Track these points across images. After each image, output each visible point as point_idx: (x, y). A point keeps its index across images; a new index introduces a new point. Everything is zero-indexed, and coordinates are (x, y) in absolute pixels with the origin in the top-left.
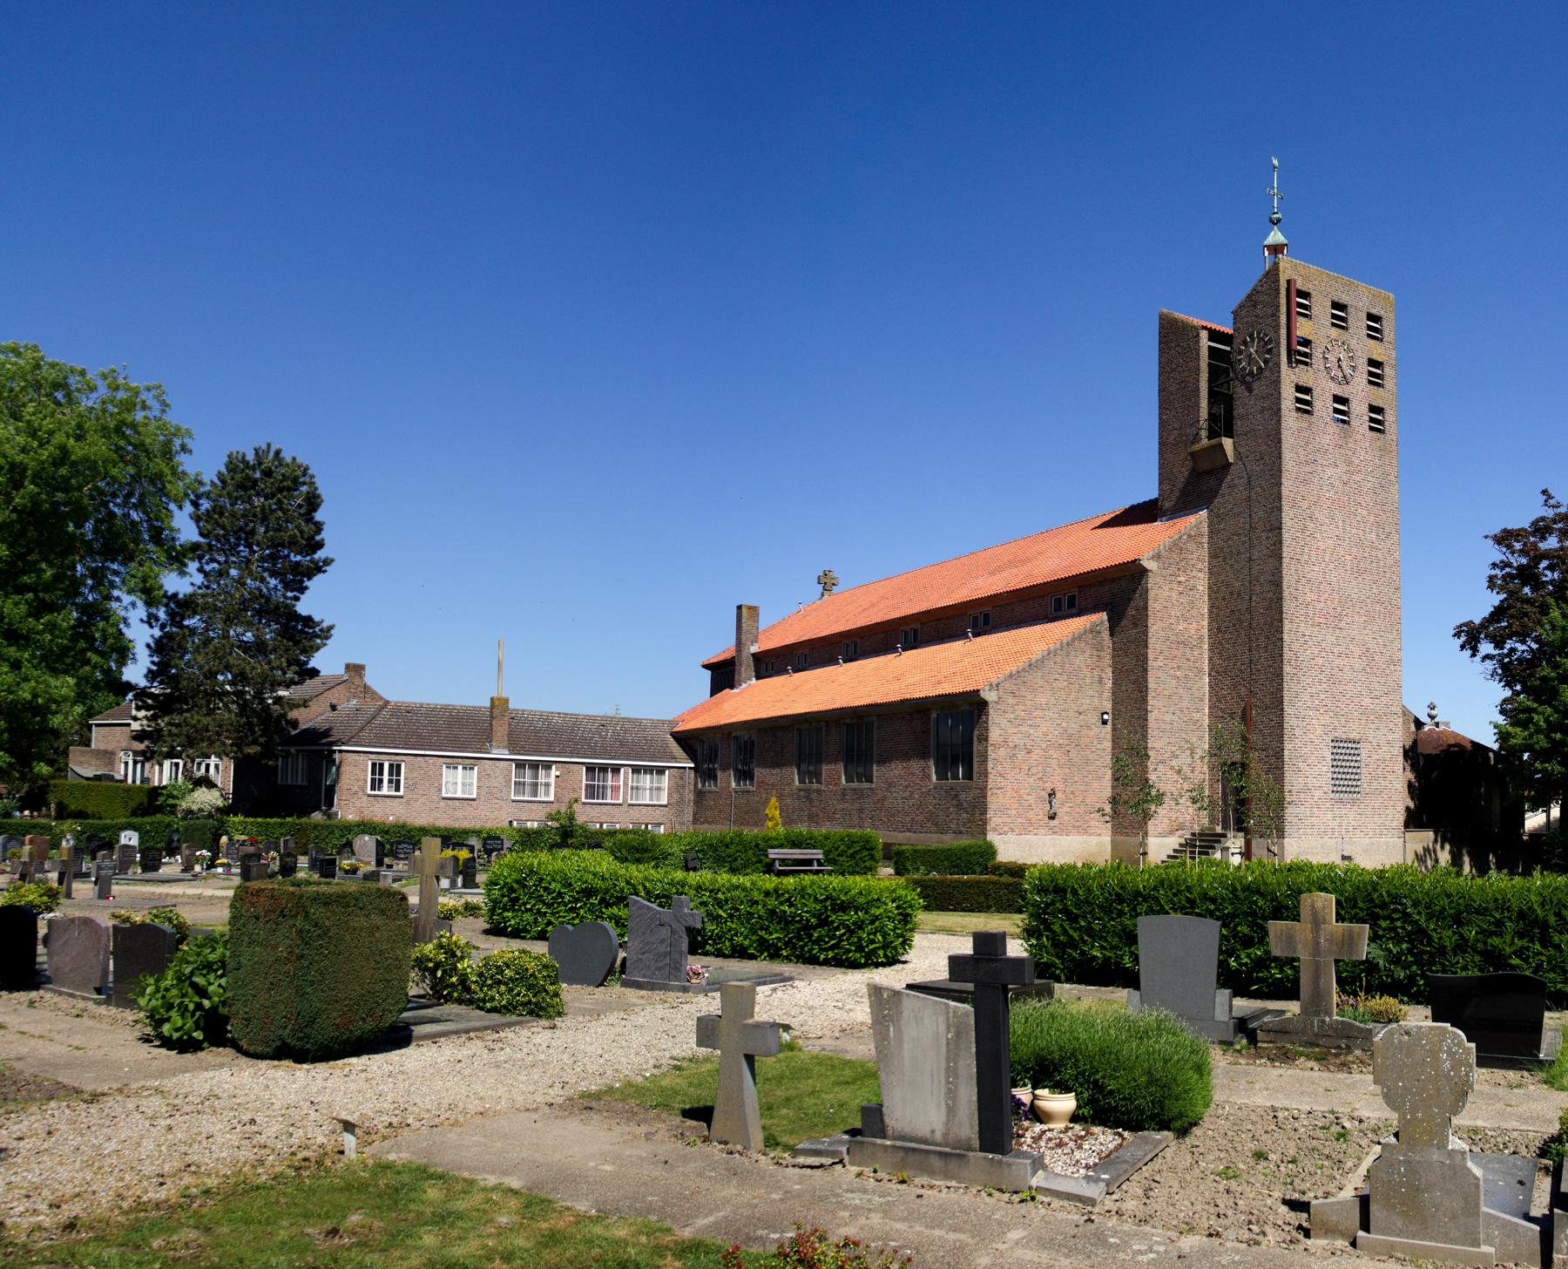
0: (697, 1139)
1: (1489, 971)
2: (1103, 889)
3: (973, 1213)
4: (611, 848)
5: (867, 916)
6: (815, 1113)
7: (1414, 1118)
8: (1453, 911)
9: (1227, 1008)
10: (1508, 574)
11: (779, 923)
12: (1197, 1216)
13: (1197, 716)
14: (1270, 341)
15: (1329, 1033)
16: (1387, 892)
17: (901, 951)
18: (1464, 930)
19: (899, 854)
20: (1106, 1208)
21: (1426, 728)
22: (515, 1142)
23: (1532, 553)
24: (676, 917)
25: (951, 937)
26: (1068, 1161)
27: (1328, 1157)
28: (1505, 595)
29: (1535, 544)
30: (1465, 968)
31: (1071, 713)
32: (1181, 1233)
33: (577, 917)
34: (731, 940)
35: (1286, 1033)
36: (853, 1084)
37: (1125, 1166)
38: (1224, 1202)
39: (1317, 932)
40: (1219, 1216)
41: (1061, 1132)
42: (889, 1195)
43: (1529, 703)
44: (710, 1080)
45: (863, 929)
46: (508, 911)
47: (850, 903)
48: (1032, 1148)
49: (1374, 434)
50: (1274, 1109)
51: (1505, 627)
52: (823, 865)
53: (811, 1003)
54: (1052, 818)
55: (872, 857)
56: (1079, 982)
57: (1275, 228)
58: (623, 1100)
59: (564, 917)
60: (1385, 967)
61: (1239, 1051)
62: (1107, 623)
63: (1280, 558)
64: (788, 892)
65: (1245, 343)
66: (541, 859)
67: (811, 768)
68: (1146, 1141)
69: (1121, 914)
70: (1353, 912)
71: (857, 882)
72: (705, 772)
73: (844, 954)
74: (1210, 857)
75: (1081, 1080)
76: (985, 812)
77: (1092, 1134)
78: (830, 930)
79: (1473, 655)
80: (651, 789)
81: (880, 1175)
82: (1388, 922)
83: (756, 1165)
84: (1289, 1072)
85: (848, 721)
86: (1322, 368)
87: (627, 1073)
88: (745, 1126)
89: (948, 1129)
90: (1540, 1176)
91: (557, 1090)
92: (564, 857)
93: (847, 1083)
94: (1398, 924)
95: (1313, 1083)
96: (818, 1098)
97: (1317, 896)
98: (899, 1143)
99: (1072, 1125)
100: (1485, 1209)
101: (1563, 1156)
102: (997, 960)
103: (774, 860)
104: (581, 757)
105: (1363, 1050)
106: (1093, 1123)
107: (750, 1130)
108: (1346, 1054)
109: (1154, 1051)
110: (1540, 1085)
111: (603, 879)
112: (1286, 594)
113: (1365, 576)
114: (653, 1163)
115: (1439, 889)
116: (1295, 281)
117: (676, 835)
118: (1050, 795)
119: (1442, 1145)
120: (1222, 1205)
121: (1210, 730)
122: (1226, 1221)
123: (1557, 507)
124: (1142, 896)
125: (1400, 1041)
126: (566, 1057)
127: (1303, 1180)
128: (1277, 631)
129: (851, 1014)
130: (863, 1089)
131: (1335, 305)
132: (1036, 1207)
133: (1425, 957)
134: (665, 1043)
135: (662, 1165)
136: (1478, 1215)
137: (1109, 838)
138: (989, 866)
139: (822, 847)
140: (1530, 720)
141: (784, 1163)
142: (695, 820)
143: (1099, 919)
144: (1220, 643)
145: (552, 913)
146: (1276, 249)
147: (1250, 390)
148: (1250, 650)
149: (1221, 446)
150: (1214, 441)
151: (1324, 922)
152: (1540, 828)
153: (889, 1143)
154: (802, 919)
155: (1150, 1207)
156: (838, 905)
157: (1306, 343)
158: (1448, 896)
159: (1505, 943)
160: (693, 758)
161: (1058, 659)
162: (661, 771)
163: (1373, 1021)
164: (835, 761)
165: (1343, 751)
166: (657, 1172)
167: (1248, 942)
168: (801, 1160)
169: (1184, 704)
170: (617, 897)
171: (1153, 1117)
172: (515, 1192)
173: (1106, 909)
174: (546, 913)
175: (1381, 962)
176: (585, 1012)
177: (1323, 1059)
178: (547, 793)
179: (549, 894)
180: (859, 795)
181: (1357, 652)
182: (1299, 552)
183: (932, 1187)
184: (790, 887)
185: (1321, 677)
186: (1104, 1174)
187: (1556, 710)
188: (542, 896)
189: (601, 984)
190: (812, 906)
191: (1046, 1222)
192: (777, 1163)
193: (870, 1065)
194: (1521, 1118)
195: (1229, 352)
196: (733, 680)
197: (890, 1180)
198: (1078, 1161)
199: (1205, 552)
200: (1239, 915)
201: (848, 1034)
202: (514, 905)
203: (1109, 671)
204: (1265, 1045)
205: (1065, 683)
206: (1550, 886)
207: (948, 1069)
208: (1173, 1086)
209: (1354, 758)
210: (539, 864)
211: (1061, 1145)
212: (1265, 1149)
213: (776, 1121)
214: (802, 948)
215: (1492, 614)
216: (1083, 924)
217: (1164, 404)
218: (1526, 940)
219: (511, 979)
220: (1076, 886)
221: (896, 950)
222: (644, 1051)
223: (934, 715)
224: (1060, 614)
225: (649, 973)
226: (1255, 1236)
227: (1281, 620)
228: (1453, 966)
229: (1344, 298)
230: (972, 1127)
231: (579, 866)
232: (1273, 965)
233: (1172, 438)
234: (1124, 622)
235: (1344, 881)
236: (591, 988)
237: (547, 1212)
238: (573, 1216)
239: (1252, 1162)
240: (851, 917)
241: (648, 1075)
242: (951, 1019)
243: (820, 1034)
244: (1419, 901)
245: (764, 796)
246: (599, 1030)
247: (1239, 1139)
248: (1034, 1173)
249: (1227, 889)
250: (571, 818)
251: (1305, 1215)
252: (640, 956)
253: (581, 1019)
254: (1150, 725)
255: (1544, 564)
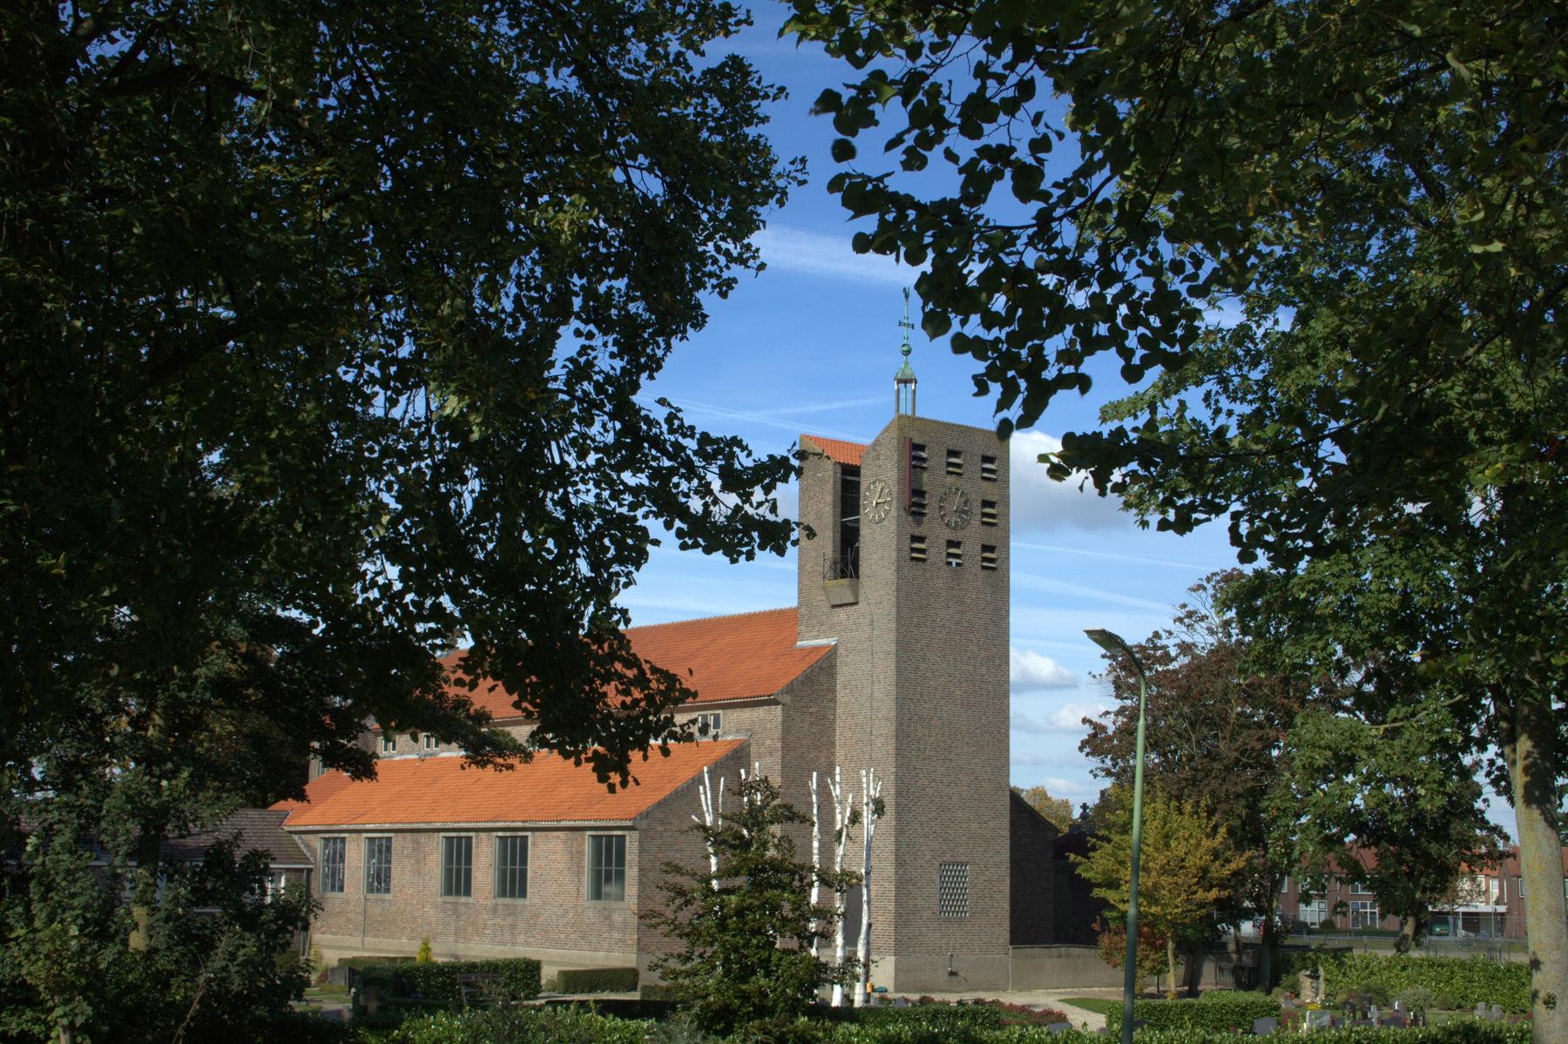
49: (986, 572)
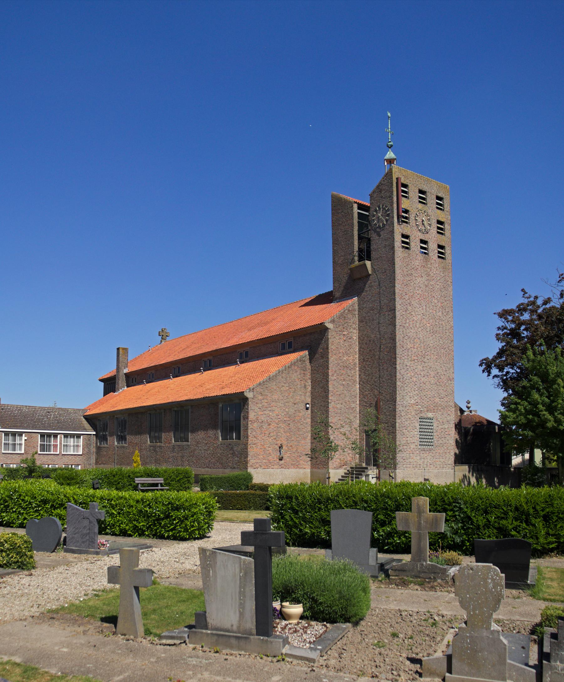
0: (110, 633)
1: (500, 538)
2: (311, 496)
3: (253, 668)
4: (55, 478)
5: (190, 513)
6: (169, 617)
7: (474, 613)
8: (483, 507)
9: (375, 558)
10: (505, 333)
11: (144, 517)
12: (366, 667)
13: (353, 405)
14: (388, 210)
15: (425, 571)
16: (452, 497)
17: (207, 531)
18: (488, 516)
19: (202, 480)
20: (320, 664)
21: (465, 414)
22: (15, 637)
23: (517, 322)
24: (91, 514)
25: (231, 523)
26: (300, 640)
27: (428, 635)
28: (505, 344)
29: (518, 317)
30: (489, 536)
31: (291, 404)
32: (358, 676)
33: (39, 515)
34: (119, 526)
35: (404, 571)
36: (187, 602)
37: (329, 642)
38: (378, 659)
39: (420, 518)
40: (376, 667)
41: (296, 625)
42: (210, 659)
43: (516, 400)
44: (114, 601)
45: (188, 520)
46: (4, 512)
47: (181, 506)
48: (281, 633)
49: (440, 260)
50: (400, 611)
51: (504, 361)
52: (163, 486)
53: (162, 560)
54: (281, 459)
55: (189, 482)
56: (299, 546)
57: (390, 150)
58: (70, 613)
59: (33, 515)
60: (450, 536)
61: (381, 581)
62: (308, 356)
63: (395, 326)
64: (148, 500)
65: (376, 211)
66: (20, 483)
67: (156, 434)
68: (338, 628)
69: (320, 509)
70: (435, 507)
71: (184, 495)
72: (101, 438)
73: (178, 533)
74: (360, 480)
75: (306, 597)
76: (246, 457)
77: (311, 625)
78: (170, 521)
79: (489, 375)
80: (74, 446)
81: (205, 649)
82: (452, 512)
83: (141, 644)
84: (406, 591)
85: (176, 409)
86: (414, 225)
87: (71, 599)
88: (135, 624)
89: (240, 624)
90: (532, 644)
91: (35, 609)
92: (32, 483)
93: (184, 601)
94: (457, 513)
95: (418, 597)
96: (170, 609)
97: (420, 498)
98: (214, 632)
99: (300, 621)
100: (509, 661)
101: (543, 634)
102: (266, 534)
103: (138, 484)
104: (38, 429)
105: (442, 579)
106: (311, 619)
107: (137, 626)
108: (434, 582)
109: (343, 581)
110: (528, 597)
111: (52, 494)
112: (398, 344)
113: (436, 334)
114: (88, 647)
115: (476, 495)
116: (400, 178)
117: (87, 470)
118: (280, 447)
119: (488, 628)
120: (378, 661)
121: (360, 413)
122: (380, 669)
123: (529, 298)
124: (331, 500)
125: (468, 573)
126: (38, 591)
127: (416, 647)
128: (393, 363)
129: (184, 565)
130: (193, 604)
131: (421, 192)
132: (285, 664)
133: (470, 531)
134: (90, 582)
135: (93, 648)
136: (505, 664)
137: (309, 470)
138: (249, 485)
139: (163, 476)
140: (517, 409)
141: (155, 643)
142: (97, 463)
143: (309, 513)
144: (365, 367)
145: (26, 513)
146: (390, 161)
147: (379, 235)
148: (379, 371)
149: (365, 265)
150: (361, 263)
151: (424, 512)
152: (519, 464)
153: (209, 632)
154: (156, 515)
155: (342, 663)
156: (175, 507)
157: (406, 211)
158: (481, 499)
159: (508, 524)
160: (95, 429)
161: (284, 375)
162: (78, 436)
163: (447, 565)
164: (169, 431)
165: (425, 424)
166: (91, 651)
167: (383, 524)
168: (164, 641)
169: (347, 399)
170: (59, 504)
171: (341, 616)
172: (18, 665)
173: (313, 507)
174: (23, 513)
175: (448, 534)
176: (47, 566)
177: (422, 584)
178: (20, 449)
179: (25, 503)
180: (182, 448)
181: (433, 374)
182: (404, 322)
183: (231, 655)
184: (149, 498)
185: (415, 387)
186: (319, 646)
187: (530, 403)
188: (21, 504)
189: (54, 551)
190: (161, 507)
191: (291, 672)
192: (152, 643)
193: (195, 591)
194: (521, 614)
195: (368, 216)
196: (115, 388)
197: (210, 652)
198: (305, 640)
199: (357, 319)
200: (379, 509)
201: (182, 576)
202: (7, 509)
203: (309, 381)
204: (393, 578)
205: (287, 388)
206: (530, 493)
207: (240, 592)
208: (352, 599)
209: (430, 427)
210: (19, 487)
211: (296, 631)
212: (397, 632)
213: (149, 621)
214: (156, 530)
215: (498, 353)
216: (301, 515)
217: (335, 242)
218: (519, 521)
219: (8, 549)
220: (297, 495)
221: (205, 531)
222: (79, 587)
223: (220, 405)
224: (284, 351)
225: (78, 544)
226: (395, 677)
227: (395, 358)
228: (483, 536)
229: (425, 188)
230: (252, 622)
231: (39, 487)
232: (395, 535)
233: (340, 261)
234: (317, 356)
235: (430, 491)
236: (48, 554)
237: (35, 674)
238: (49, 676)
239: (391, 639)
240: (181, 513)
241: (82, 599)
242: (242, 566)
243: (168, 575)
244: (467, 501)
245: (132, 449)
246: (55, 576)
247: (384, 627)
248: (284, 646)
249: (373, 495)
250: (34, 462)
251: (419, 666)
252: (74, 536)
253: (45, 570)
254: (330, 410)
255: (523, 327)
